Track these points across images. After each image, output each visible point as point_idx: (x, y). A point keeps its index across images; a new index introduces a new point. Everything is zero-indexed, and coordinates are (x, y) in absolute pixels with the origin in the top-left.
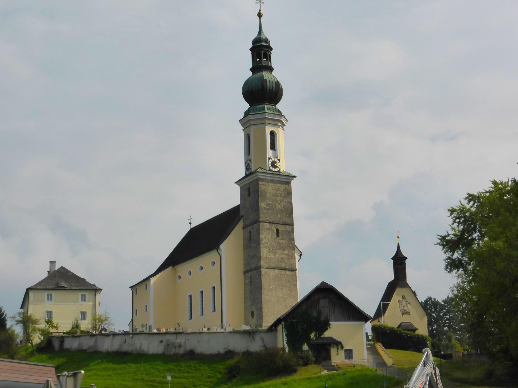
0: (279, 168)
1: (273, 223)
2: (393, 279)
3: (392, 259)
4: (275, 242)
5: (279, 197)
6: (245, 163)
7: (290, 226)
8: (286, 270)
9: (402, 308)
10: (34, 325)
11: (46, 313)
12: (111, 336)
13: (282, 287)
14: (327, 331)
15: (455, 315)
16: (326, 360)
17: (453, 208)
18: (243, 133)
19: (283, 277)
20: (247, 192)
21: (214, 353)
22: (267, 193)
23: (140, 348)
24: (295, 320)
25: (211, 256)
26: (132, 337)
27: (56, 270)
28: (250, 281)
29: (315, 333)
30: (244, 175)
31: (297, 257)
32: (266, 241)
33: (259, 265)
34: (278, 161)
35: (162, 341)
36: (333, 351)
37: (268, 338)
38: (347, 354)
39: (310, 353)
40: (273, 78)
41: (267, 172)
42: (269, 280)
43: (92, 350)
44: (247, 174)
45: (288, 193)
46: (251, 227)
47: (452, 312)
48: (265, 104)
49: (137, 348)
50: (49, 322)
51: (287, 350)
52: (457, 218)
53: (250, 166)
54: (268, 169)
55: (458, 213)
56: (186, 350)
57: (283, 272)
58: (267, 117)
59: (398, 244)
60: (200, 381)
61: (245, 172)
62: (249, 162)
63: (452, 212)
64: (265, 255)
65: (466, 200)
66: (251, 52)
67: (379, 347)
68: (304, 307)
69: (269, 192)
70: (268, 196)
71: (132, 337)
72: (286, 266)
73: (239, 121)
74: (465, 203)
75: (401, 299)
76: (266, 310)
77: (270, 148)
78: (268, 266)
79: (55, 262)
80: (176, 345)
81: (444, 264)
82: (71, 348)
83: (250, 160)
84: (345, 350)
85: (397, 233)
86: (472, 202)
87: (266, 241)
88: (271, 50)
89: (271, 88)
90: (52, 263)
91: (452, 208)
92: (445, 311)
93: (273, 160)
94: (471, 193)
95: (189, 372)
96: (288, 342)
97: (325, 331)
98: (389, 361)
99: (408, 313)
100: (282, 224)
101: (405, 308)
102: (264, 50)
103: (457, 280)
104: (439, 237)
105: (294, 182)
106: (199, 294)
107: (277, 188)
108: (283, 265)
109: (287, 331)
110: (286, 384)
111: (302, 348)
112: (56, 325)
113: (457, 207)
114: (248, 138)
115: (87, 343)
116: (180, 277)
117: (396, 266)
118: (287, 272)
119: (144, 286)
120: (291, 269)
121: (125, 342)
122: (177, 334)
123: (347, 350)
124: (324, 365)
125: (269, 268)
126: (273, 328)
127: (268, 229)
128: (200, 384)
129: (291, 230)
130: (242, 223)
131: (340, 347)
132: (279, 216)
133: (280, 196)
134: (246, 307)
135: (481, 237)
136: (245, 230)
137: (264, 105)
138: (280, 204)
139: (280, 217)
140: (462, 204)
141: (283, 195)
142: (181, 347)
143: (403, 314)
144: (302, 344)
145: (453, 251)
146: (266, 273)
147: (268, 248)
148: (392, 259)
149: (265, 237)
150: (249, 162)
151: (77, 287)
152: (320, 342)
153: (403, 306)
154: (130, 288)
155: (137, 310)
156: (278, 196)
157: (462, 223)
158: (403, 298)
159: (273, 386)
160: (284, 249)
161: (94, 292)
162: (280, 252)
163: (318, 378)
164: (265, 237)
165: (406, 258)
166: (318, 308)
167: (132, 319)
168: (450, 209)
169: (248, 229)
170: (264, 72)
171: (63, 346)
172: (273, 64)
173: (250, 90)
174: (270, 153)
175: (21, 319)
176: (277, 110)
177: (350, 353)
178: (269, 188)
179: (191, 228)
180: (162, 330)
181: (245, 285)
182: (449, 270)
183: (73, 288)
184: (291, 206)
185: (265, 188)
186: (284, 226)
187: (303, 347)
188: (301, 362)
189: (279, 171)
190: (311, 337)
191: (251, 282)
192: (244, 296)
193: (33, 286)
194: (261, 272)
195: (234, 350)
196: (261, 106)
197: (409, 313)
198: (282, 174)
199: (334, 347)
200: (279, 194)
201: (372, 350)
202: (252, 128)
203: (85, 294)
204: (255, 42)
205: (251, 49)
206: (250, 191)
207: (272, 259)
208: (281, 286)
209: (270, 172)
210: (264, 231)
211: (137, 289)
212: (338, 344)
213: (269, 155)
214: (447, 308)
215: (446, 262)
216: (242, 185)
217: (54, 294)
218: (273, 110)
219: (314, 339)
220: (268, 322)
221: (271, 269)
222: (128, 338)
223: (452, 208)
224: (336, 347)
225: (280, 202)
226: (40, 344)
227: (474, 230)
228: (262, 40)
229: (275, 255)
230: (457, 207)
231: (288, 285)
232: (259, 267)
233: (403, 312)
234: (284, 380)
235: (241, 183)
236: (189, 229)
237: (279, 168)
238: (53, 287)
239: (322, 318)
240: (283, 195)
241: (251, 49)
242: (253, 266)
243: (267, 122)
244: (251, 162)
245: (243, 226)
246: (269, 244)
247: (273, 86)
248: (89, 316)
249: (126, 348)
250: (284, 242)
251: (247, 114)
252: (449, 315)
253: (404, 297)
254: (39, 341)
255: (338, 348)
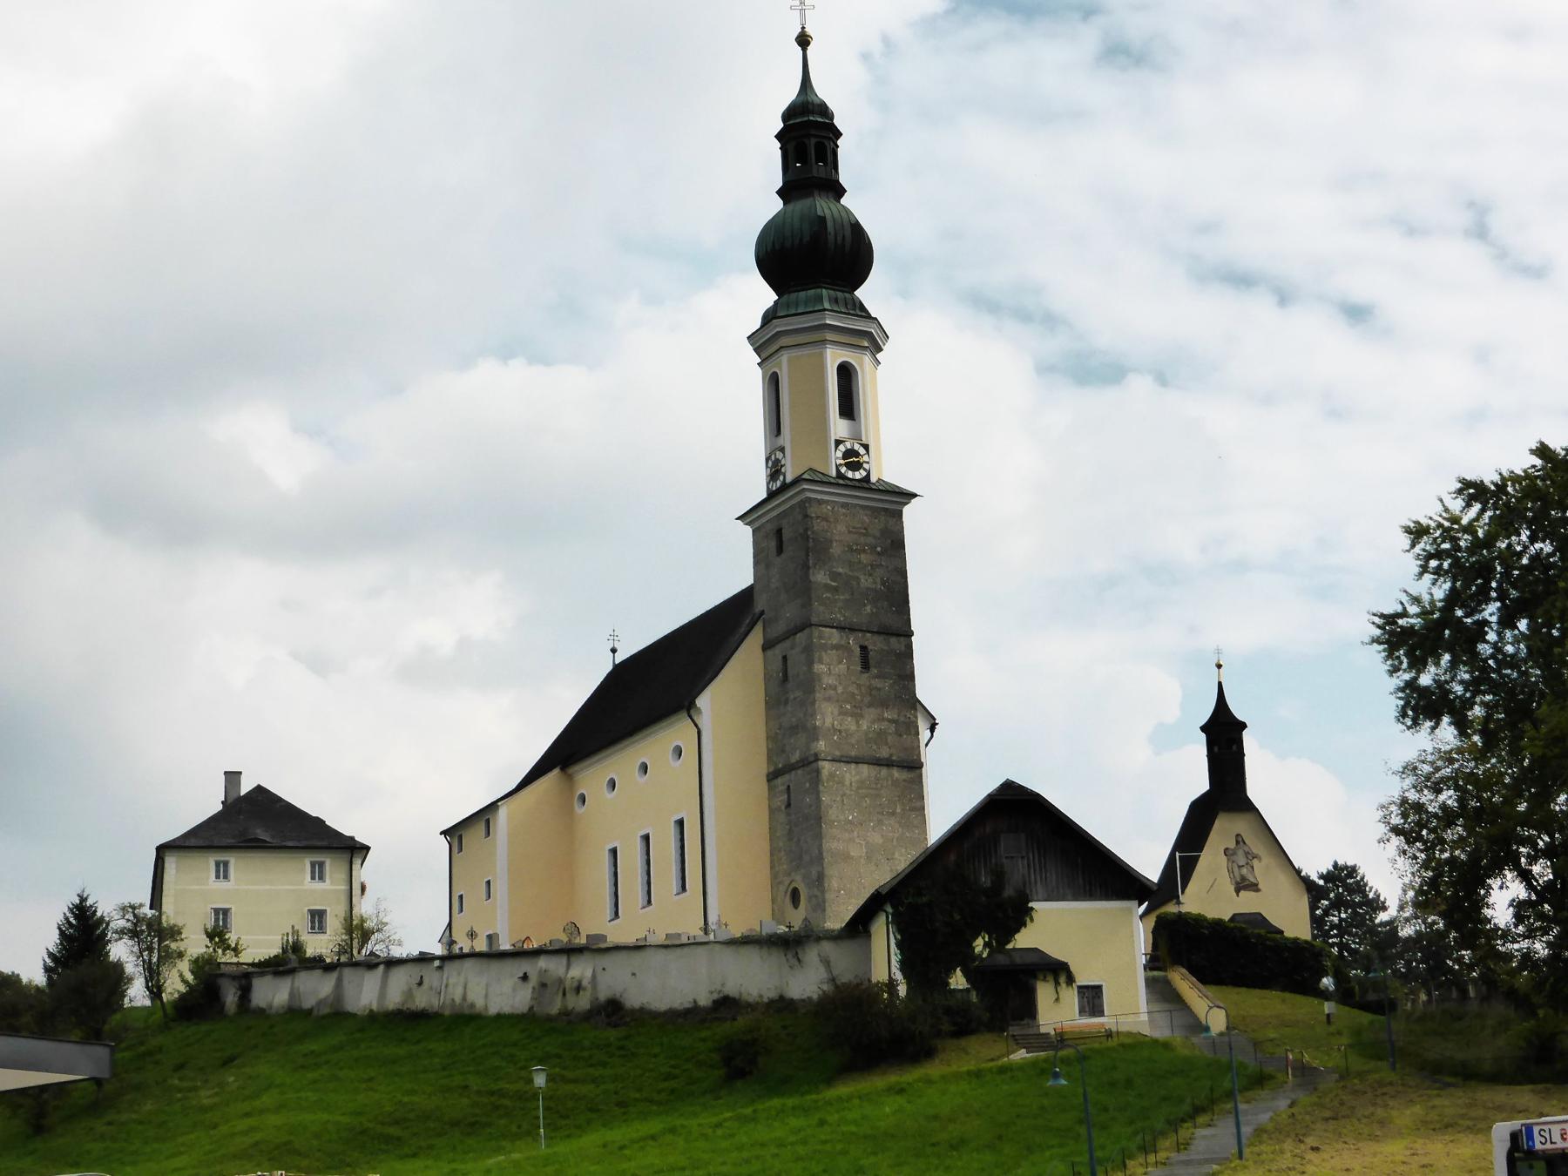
0: (865, 470)
1: (852, 630)
2: (1208, 788)
3: (1203, 729)
4: (857, 685)
5: (867, 553)
6: (767, 460)
7: (902, 639)
8: (893, 766)
9: (1236, 870)
10: (167, 942)
11: (213, 914)
12: (382, 967)
13: (880, 817)
14: (1023, 930)
15: (1355, 913)
16: (1022, 1019)
17: (1417, 523)
18: (759, 371)
19: (882, 786)
20: (773, 544)
21: (682, 1008)
22: (831, 541)
23: (464, 998)
24: (925, 899)
25: (677, 732)
26: (440, 968)
27: (243, 793)
28: (786, 800)
29: (987, 936)
30: (764, 495)
31: (924, 734)
32: (828, 680)
33: (812, 752)
34: (862, 451)
35: (525, 978)
36: (1044, 992)
37: (843, 959)
38: (1085, 999)
39: (974, 997)
40: (843, 214)
41: (833, 481)
42: (842, 796)
43: (326, 1010)
44: (774, 488)
45: (892, 541)
46: (787, 644)
47: (1347, 905)
48: (822, 287)
49: (453, 1000)
50: (217, 934)
51: (902, 990)
52: (1430, 556)
53: (782, 466)
54: (834, 473)
55: (1435, 539)
56: (597, 999)
57: (884, 771)
58: (828, 322)
59: (1220, 684)
60: (639, 1090)
61: (768, 484)
62: (778, 453)
63: (1415, 538)
64: (828, 721)
65: (1457, 497)
66: (779, 145)
67: (1182, 981)
68: (952, 857)
69: (837, 538)
70: (836, 550)
71: (440, 968)
72: (891, 755)
73: (748, 338)
74: (1456, 505)
75: (1232, 845)
76: (835, 884)
77: (840, 414)
78: (837, 753)
79: (240, 773)
80: (568, 984)
81: (1394, 703)
82: (270, 1007)
83: (782, 450)
84: (1080, 987)
85: (1215, 653)
86: (1477, 507)
87: (831, 681)
88: (838, 138)
89: (839, 241)
90: (232, 778)
91: (1414, 522)
92: (1326, 903)
93: (849, 447)
94: (1470, 477)
95: (604, 1065)
96: (905, 966)
97: (1018, 931)
98: (1217, 1021)
99: (1254, 887)
100: (878, 633)
101: (1244, 871)
102: (816, 136)
103: (1401, 782)
104: (1377, 620)
105: (909, 512)
106: (638, 845)
107: (860, 528)
108: (884, 753)
109: (900, 930)
110: (901, 1091)
111: (948, 984)
112: (233, 945)
113: (1431, 518)
114: (773, 384)
115: (315, 989)
116: (583, 799)
117: (1216, 749)
118: (896, 773)
119: (482, 826)
120: (905, 765)
121: (420, 984)
122: (570, 951)
123: (1087, 987)
124: (1015, 1034)
125: (840, 761)
126: (859, 926)
127: (836, 647)
128: (636, 1100)
129: (903, 648)
130: (761, 635)
131: (1062, 979)
132: (868, 608)
133: (869, 551)
134: (774, 876)
135: (1507, 621)
136: (770, 653)
137: (819, 290)
138: (870, 575)
139: (872, 610)
140: (1447, 510)
141: (879, 549)
142: (581, 992)
143: (1238, 891)
144: (950, 971)
145: (1418, 664)
146: (832, 775)
147: (838, 701)
148: (1203, 729)
149: (829, 669)
150: (779, 455)
151: (299, 841)
152: (1001, 959)
153: (1240, 867)
154: (441, 834)
155: (461, 897)
156: (864, 551)
157: (1447, 572)
158: (1238, 842)
159: (860, 1098)
160: (884, 704)
161: (347, 856)
162: (871, 713)
163: (1003, 1070)
164: (829, 669)
165: (1243, 726)
166: (993, 861)
167: (450, 925)
168: (1409, 527)
169: (777, 652)
170: (817, 198)
171: (250, 1001)
172: (844, 179)
173: (777, 247)
174: (839, 427)
175: (129, 925)
176: (858, 305)
177: (1093, 998)
178: (839, 527)
179: (617, 662)
180: (528, 944)
181: (772, 811)
182: (1409, 723)
183: (290, 844)
184: (903, 580)
185: (826, 527)
186: (881, 638)
187: (950, 981)
188: (946, 1027)
189: (867, 478)
190: (976, 951)
191: (789, 805)
192: (771, 845)
193: (174, 840)
194: (818, 771)
195: (741, 994)
196: (811, 292)
197: (1255, 888)
198: (874, 487)
199: (1045, 979)
200: (866, 544)
201: (1161, 991)
202: (784, 358)
203: (323, 859)
204: (788, 115)
205: (779, 137)
206: (784, 539)
207: (851, 735)
208: (878, 813)
209: (841, 482)
210: (826, 651)
211: (460, 838)
212: (1058, 971)
213: (836, 434)
214: (1332, 895)
215: (1400, 698)
216: (757, 525)
217: (235, 861)
218: (846, 304)
219: (985, 955)
220: (839, 914)
221: (848, 762)
222: (430, 974)
223: (1414, 522)
224: (1050, 978)
225: (869, 568)
226: (183, 997)
227: (1483, 597)
228: (810, 107)
229: (857, 722)
230: (1431, 518)
231: (898, 810)
232: (812, 759)
233: (1237, 883)
234: (893, 1078)
235: (754, 519)
236: (610, 668)
237: (865, 470)
238: (230, 841)
239: (1009, 892)
240: (879, 549)
241: (779, 137)
242: (795, 757)
243: (828, 338)
244: (784, 453)
245: (762, 642)
246: (840, 690)
247: (844, 236)
248: (334, 923)
249: (422, 1001)
250: (885, 685)
251: (769, 317)
252: (1340, 913)
253: (1241, 840)
254: (182, 988)
255: (1057, 983)
